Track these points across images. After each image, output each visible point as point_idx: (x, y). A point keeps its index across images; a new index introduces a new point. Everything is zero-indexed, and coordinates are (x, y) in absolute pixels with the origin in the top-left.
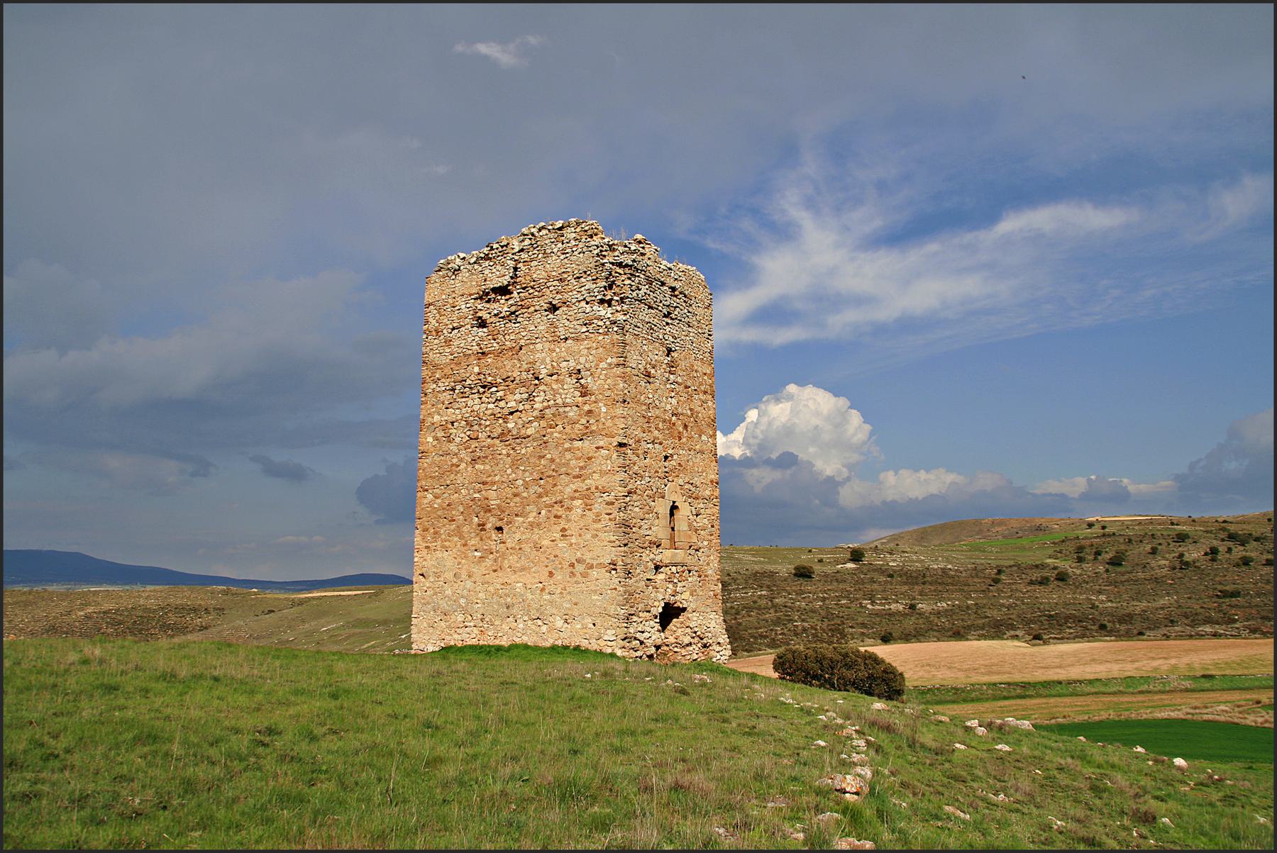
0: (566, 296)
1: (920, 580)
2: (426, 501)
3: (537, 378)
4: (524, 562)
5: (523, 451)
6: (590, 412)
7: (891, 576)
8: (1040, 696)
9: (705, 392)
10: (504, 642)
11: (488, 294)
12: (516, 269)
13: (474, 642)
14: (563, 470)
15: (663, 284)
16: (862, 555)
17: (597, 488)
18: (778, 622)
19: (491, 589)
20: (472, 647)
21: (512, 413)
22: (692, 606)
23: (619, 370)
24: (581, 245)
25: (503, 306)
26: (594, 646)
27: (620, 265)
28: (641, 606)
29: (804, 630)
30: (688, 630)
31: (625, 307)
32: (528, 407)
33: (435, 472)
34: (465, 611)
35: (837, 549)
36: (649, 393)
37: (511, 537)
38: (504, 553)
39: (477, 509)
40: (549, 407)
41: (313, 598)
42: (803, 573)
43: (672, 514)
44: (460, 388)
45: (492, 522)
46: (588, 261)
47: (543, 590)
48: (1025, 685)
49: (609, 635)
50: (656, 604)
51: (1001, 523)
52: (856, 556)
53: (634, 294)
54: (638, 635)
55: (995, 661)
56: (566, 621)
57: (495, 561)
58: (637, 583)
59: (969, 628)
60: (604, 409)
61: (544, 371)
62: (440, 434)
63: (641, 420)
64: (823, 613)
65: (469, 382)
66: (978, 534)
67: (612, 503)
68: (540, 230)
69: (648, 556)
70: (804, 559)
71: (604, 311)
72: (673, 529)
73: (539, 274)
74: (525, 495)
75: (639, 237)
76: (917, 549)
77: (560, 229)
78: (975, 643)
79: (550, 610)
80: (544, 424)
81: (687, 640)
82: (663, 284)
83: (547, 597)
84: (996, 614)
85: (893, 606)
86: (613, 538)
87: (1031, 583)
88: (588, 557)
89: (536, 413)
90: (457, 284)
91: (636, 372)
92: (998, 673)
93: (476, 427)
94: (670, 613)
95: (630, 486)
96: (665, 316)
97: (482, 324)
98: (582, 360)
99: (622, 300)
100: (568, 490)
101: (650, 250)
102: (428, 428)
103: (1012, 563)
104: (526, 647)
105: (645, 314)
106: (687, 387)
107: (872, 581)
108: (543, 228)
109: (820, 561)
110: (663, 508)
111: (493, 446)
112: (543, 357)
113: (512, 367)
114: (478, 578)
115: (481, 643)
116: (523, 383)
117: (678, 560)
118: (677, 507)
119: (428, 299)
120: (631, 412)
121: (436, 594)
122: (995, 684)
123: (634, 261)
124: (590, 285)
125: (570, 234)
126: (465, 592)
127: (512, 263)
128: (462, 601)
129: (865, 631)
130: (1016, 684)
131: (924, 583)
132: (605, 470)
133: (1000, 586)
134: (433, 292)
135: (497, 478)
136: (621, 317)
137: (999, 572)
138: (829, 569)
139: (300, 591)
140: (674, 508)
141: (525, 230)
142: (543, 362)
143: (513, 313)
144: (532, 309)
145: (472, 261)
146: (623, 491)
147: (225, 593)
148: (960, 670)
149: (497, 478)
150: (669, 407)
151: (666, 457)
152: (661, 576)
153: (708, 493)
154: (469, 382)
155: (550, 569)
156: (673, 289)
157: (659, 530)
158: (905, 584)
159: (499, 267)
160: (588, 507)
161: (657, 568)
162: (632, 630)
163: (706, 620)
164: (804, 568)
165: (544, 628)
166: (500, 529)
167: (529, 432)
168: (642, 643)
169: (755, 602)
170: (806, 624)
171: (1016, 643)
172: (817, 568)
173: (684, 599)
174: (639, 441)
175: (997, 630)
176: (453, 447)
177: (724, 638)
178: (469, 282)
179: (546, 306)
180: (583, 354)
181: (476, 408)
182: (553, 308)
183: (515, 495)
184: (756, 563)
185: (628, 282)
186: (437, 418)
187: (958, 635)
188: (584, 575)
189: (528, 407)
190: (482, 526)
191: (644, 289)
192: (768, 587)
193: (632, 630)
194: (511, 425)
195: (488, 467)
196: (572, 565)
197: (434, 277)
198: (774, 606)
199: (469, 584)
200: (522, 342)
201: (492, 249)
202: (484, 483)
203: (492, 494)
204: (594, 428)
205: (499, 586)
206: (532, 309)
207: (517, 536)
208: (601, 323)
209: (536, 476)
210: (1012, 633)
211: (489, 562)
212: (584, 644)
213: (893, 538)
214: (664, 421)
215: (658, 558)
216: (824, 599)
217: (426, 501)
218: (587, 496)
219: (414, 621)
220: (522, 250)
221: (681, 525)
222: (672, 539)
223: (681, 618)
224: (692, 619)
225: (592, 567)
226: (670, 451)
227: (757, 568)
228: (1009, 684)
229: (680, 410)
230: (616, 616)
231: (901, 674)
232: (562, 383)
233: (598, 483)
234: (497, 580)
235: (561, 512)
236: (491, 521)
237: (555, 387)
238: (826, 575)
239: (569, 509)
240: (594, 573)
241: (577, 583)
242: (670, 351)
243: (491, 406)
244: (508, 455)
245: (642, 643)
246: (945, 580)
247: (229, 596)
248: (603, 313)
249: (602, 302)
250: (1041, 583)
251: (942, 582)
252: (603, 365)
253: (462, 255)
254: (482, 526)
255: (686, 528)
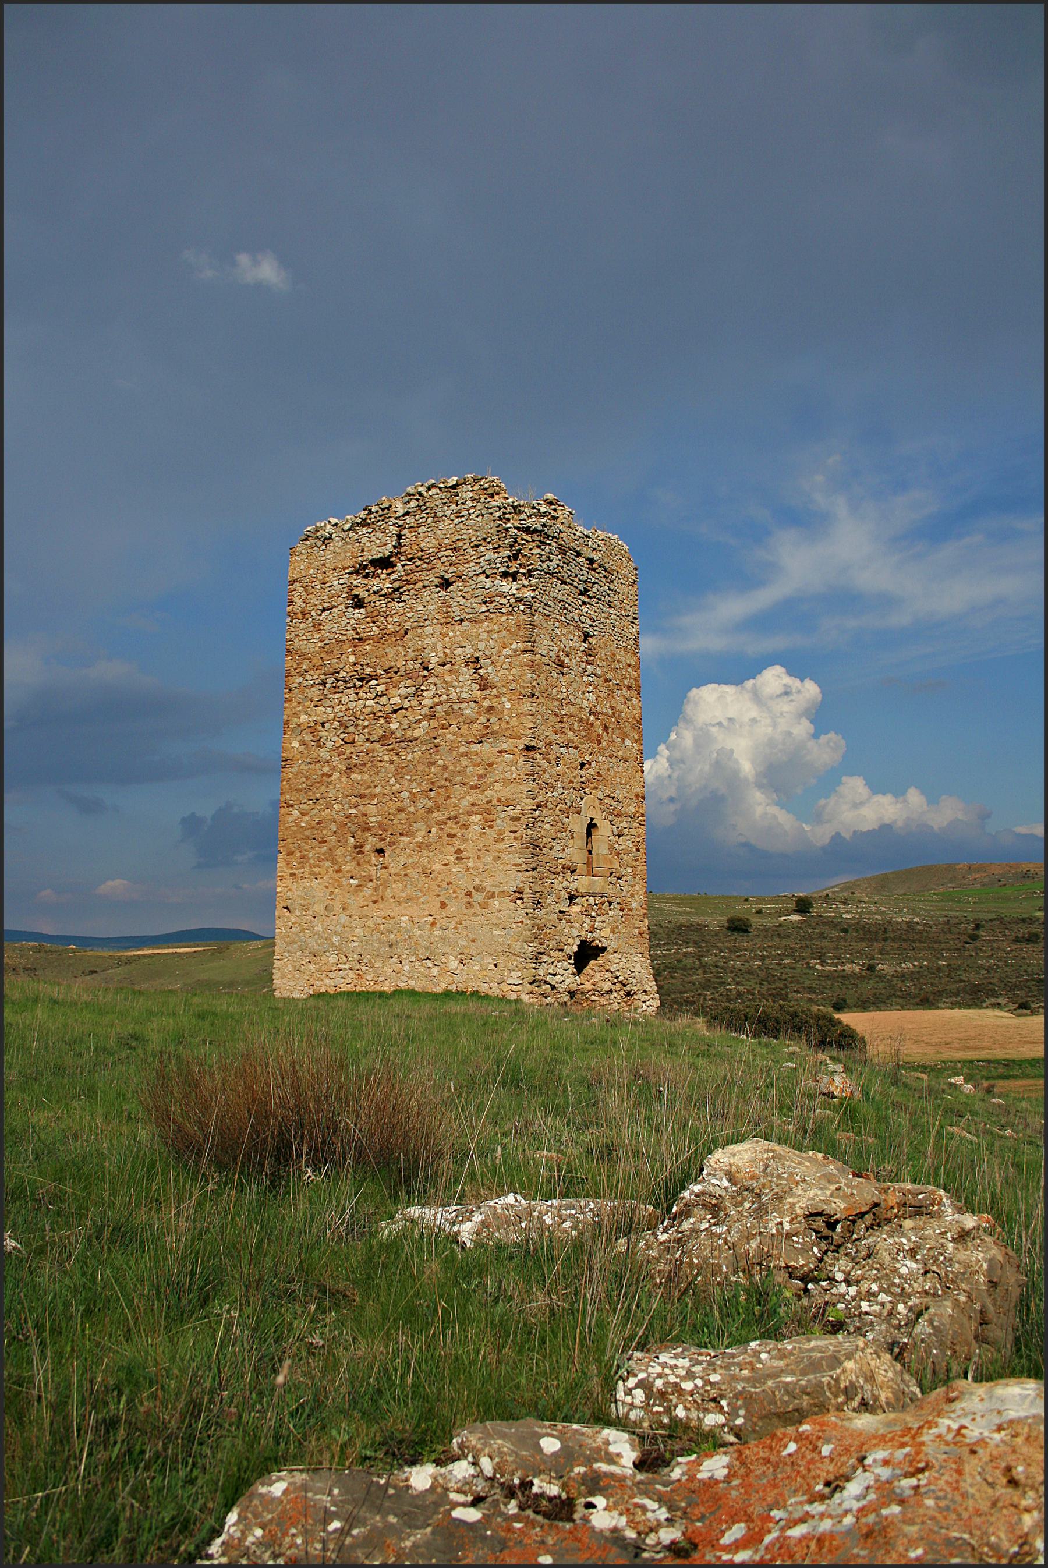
0: (461, 569)
1: (881, 936)
2: (290, 819)
3: (426, 669)
4: (410, 890)
5: (410, 757)
6: (491, 708)
7: (845, 931)
8: (1027, 1076)
9: (629, 688)
10: (387, 987)
11: (365, 567)
12: (399, 536)
13: (349, 988)
14: (459, 779)
15: (579, 554)
16: (810, 905)
17: (499, 800)
18: (707, 985)
19: (370, 923)
20: (349, 994)
21: (395, 711)
22: (614, 945)
23: (526, 658)
24: (479, 506)
25: (383, 581)
26: (496, 991)
27: (527, 530)
28: (552, 944)
29: (739, 995)
30: (609, 974)
31: (533, 581)
32: (414, 703)
33: (302, 783)
34: (338, 950)
35: (777, 899)
36: (562, 687)
37: (395, 861)
38: (386, 881)
39: (353, 828)
40: (440, 703)
41: (144, 956)
42: (738, 927)
43: (589, 834)
44: (333, 682)
45: (371, 843)
46: (487, 526)
47: (433, 924)
48: (1008, 1063)
49: (514, 977)
50: (570, 941)
51: (980, 869)
52: (803, 906)
53: (545, 566)
54: (549, 978)
55: (972, 1033)
56: (461, 962)
57: (376, 889)
58: (547, 915)
59: (940, 994)
60: (508, 706)
61: (434, 660)
62: (308, 737)
63: (553, 718)
64: (762, 975)
65: (343, 674)
66: (951, 881)
67: (518, 819)
68: (429, 489)
69: (560, 883)
70: (740, 909)
71: (508, 586)
72: (590, 852)
73: (428, 543)
74: (412, 809)
75: (550, 496)
76: (876, 898)
77: (454, 487)
78: (948, 1013)
79: (441, 948)
80: (434, 723)
81: (607, 986)
82: (579, 554)
83: (438, 933)
84: (975, 979)
85: (847, 967)
86: (519, 861)
87: (1017, 940)
88: (488, 884)
89: (425, 711)
90: (327, 556)
91: (546, 660)
92: (976, 1049)
93: (351, 729)
94: (586, 954)
95: (539, 799)
96: (581, 593)
97: (359, 603)
98: (481, 646)
99: (529, 574)
100: (464, 803)
101: (562, 513)
102: (293, 730)
103: (993, 916)
104: (412, 993)
105: (557, 591)
106: (607, 680)
107: (822, 936)
108: (433, 486)
109: (759, 912)
110: (579, 826)
111: (373, 751)
112: (433, 643)
113: (395, 656)
114: (354, 910)
115: (358, 989)
116: (409, 675)
117: (597, 889)
118: (595, 825)
119: (292, 574)
120: (541, 709)
121: (303, 930)
122: (971, 1062)
123: (544, 525)
124: (491, 555)
125: (466, 493)
126: (339, 928)
127: (394, 530)
128: (335, 939)
129: (813, 996)
130: (998, 1062)
131: (885, 940)
132: (509, 779)
133: (978, 943)
134: (299, 566)
135: (377, 790)
136: (528, 593)
137: (978, 927)
138: (769, 922)
139: (127, 948)
140: (592, 826)
141: (410, 489)
142: (434, 648)
143: (397, 590)
144: (420, 585)
145: (347, 526)
146: (531, 804)
147: (38, 950)
148: (928, 1044)
149: (377, 790)
150: (585, 704)
151: (582, 765)
152: (576, 909)
153: (632, 809)
154: (343, 674)
155: (442, 899)
156: (591, 561)
157: (574, 853)
158: (862, 940)
159: (379, 535)
160: (489, 824)
161: (571, 898)
162: (541, 972)
163: (630, 963)
164: (739, 920)
165: (435, 971)
166: (381, 851)
167: (417, 733)
168: (553, 988)
169: (679, 961)
170: (741, 988)
171: (998, 1012)
172: (755, 920)
173: (603, 936)
174: (550, 744)
175: (974, 996)
176: (324, 753)
177: (651, 986)
178: (341, 554)
179: (437, 581)
180: (480, 639)
181: (351, 705)
182: (446, 584)
183: (400, 810)
184: (680, 914)
185: (536, 551)
186: (304, 718)
187: (926, 1002)
188: (484, 906)
189: (414, 703)
190: (359, 848)
191: (556, 560)
192: (695, 942)
193: (541, 972)
194: (394, 726)
195: (366, 777)
196: (469, 894)
197: (300, 547)
198: (703, 966)
199: (343, 918)
200: (408, 625)
201: (370, 512)
202: (361, 796)
203: (372, 809)
204: (496, 728)
205: (379, 921)
206: (420, 585)
207: (402, 860)
208: (503, 601)
209: (425, 786)
210: (993, 1000)
211: (367, 892)
212: (484, 988)
213: (846, 887)
214: (580, 721)
215: (573, 886)
216: (763, 958)
217: (290, 819)
218: (487, 811)
219: (277, 964)
220: (407, 514)
221: (600, 847)
222: (589, 863)
223: (600, 960)
224: (614, 961)
225: (493, 896)
226: (588, 758)
227: (682, 920)
228: (989, 1061)
229: (599, 708)
230: (523, 955)
231: (862, 1038)
232: (457, 673)
233: (500, 795)
234: (377, 914)
235: (455, 829)
236: (370, 842)
237: (448, 678)
238: (766, 929)
239: (465, 826)
240: (496, 903)
241: (475, 915)
242: (586, 636)
243: (370, 703)
244: (391, 762)
245: (553, 988)
246: (911, 935)
247: (42, 954)
248: (506, 589)
249: (505, 575)
250: (1028, 941)
251: (908, 938)
252: (507, 651)
253: (334, 521)
254: (359, 848)
255: (606, 851)
